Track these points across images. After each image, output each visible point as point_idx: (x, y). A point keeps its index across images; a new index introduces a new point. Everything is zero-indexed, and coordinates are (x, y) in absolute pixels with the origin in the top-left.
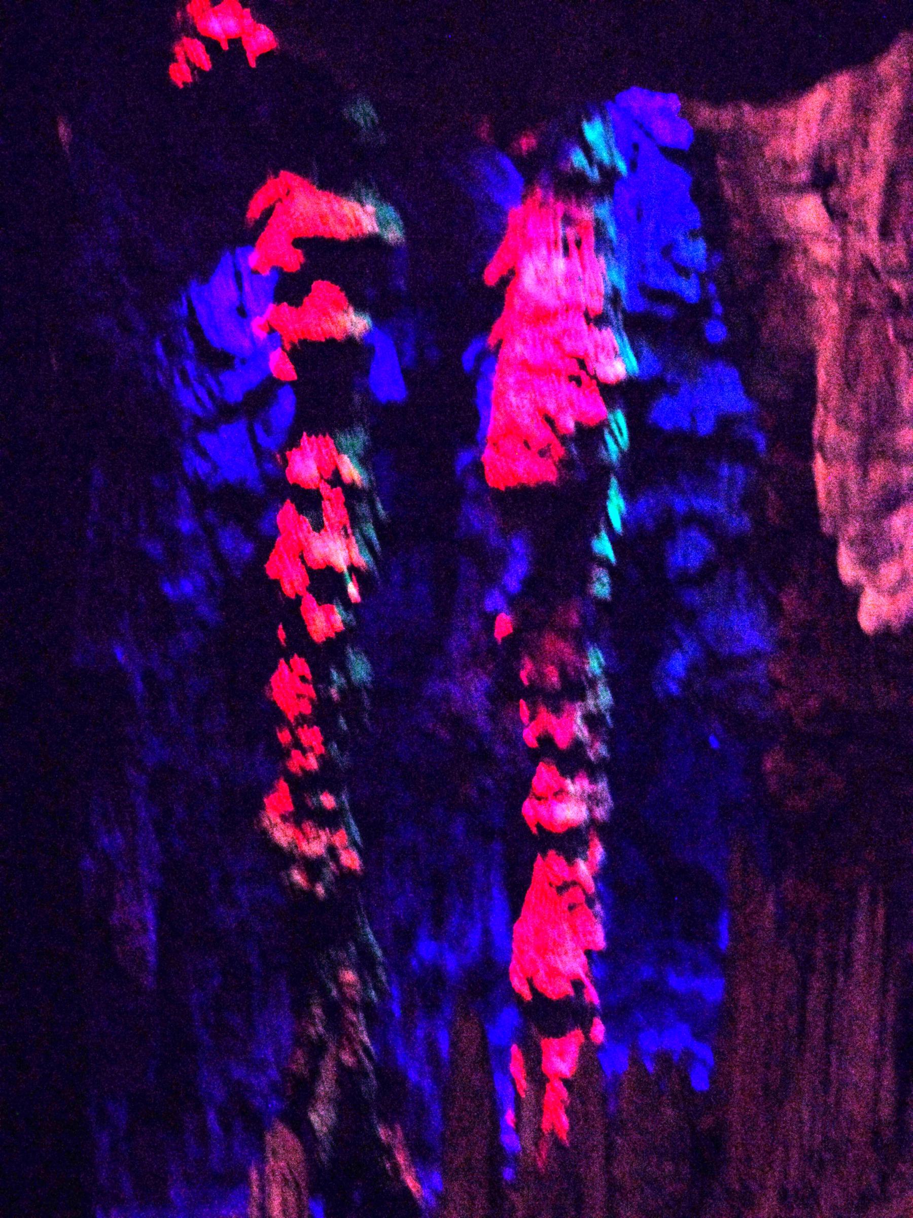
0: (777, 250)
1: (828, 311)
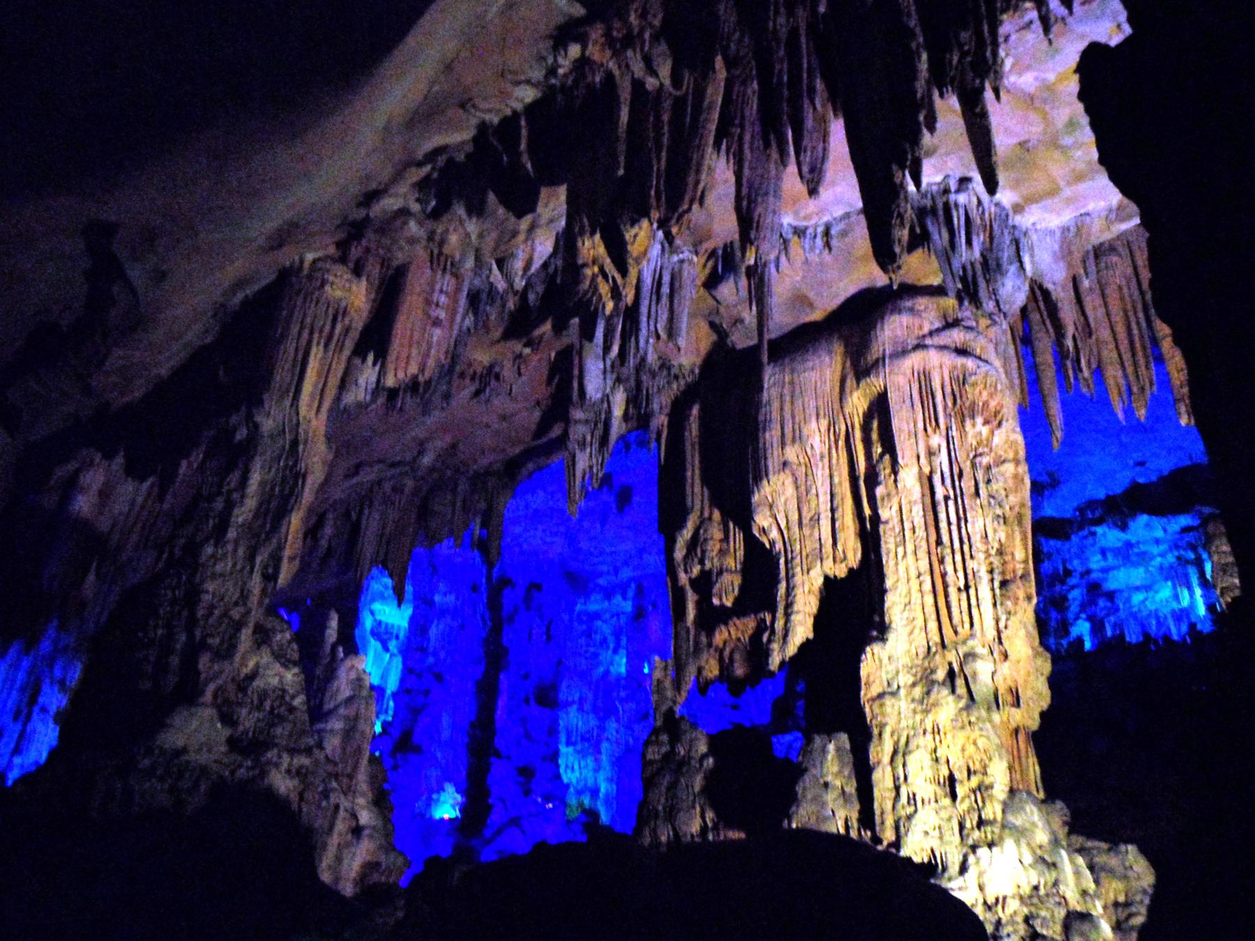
0: (380, 801)
1: (362, 777)
